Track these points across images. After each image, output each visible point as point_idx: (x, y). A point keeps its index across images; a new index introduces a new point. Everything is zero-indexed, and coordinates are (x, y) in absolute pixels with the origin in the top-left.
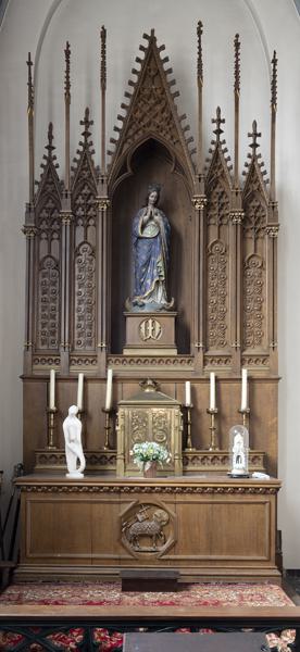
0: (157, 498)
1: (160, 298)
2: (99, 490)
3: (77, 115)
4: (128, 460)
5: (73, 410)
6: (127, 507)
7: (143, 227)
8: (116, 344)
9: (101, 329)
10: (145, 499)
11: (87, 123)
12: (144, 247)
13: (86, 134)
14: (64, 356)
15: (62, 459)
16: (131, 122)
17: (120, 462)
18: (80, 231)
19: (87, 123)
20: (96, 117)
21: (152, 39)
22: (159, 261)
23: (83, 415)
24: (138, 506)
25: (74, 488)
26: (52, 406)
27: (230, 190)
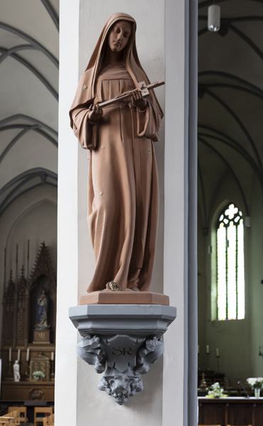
0: (39, 387)
1: (45, 325)
2: (23, 385)
3: (20, 267)
4: (33, 377)
5: (17, 362)
6: (30, 390)
7: (40, 301)
8: (31, 340)
9: (26, 335)
10: (36, 387)
11: (23, 270)
12: (40, 309)
13: (22, 273)
14: (14, 344)
15: (13, 377)
16: (37, 269)
17: (31, 377)
18: (20, 304)
19: (23, 270)
20: (26, 268)
21: (44, 244)
22: (45, 313)
23: (20, 363)
24: (34, 390)
25: (16, 384)
26: (10, 360)
27: (90, 113)
